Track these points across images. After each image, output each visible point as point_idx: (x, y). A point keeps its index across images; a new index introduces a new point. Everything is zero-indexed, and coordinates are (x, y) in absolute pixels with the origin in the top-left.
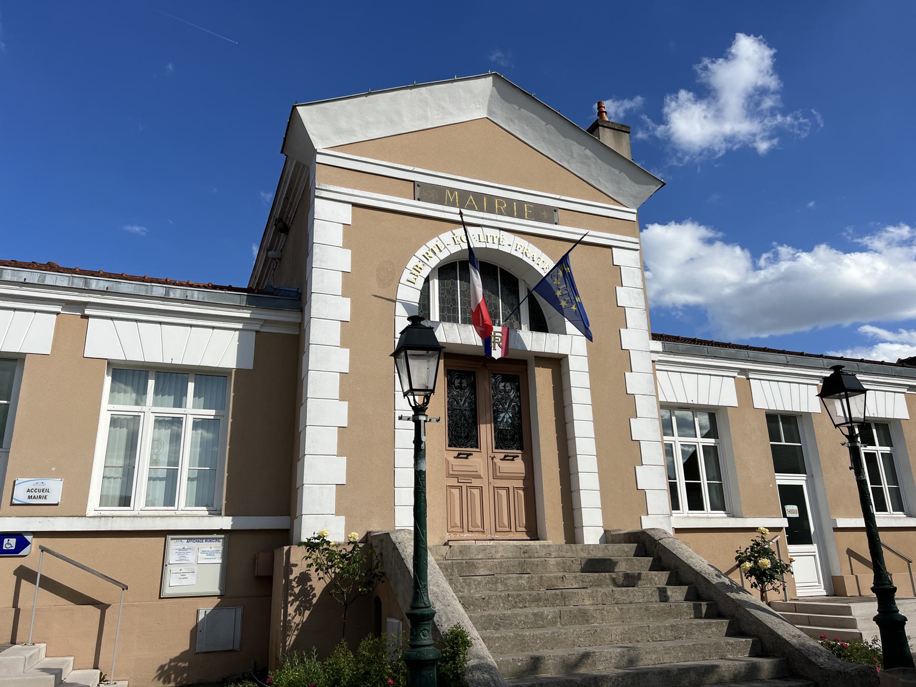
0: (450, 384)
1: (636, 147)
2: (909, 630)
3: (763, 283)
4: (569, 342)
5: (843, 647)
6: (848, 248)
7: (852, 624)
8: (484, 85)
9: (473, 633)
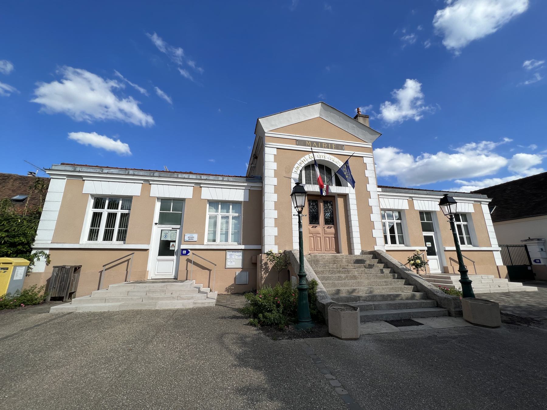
0: (309, 204)
1: (371, 122)
2: (473, 285)
3: (418, 167)
4: (348, 189)
5: (447, 290)
6: (451, 152)
7: (451, 282)
8: (318, 106)
9: (319, 281)
